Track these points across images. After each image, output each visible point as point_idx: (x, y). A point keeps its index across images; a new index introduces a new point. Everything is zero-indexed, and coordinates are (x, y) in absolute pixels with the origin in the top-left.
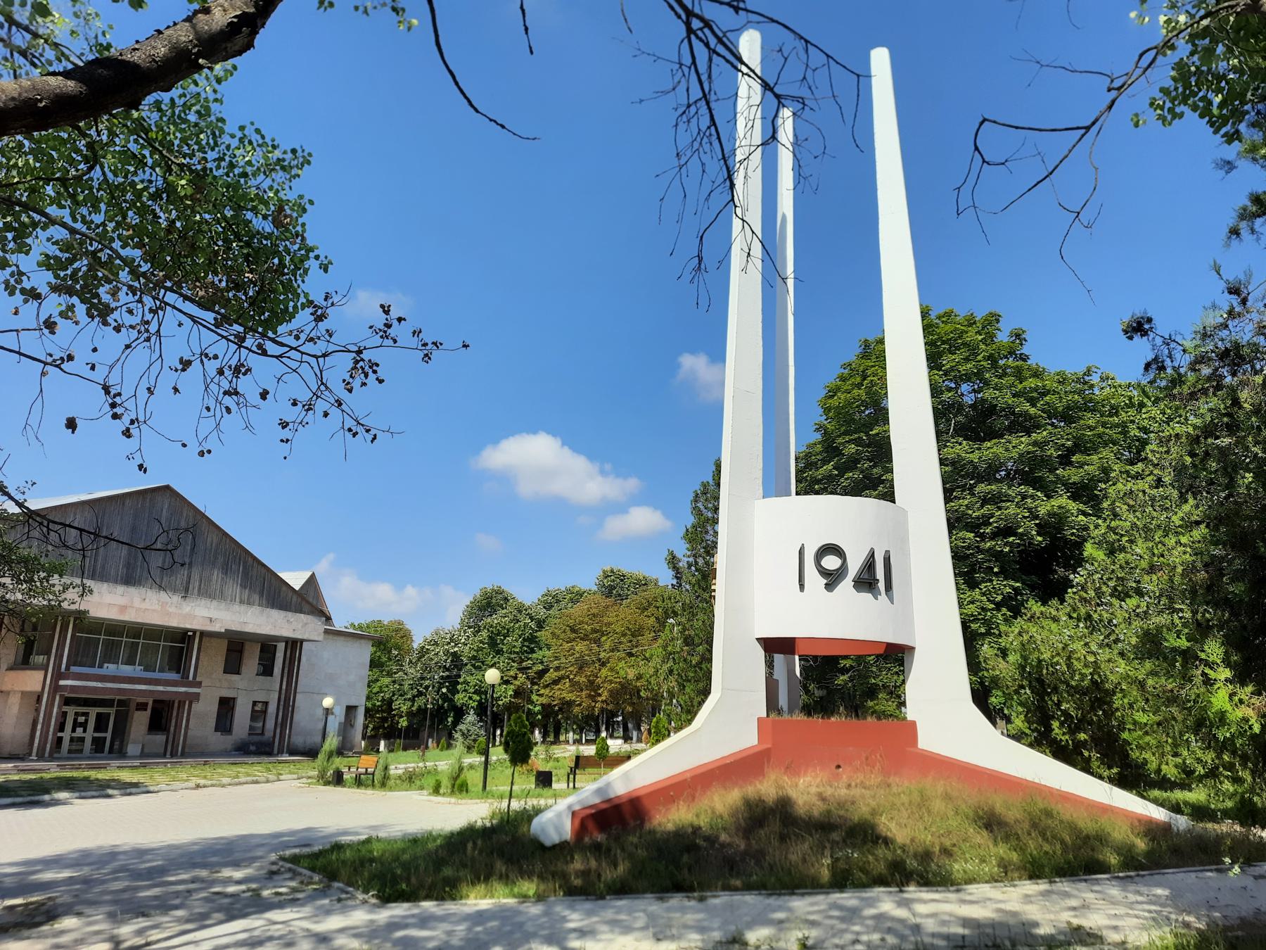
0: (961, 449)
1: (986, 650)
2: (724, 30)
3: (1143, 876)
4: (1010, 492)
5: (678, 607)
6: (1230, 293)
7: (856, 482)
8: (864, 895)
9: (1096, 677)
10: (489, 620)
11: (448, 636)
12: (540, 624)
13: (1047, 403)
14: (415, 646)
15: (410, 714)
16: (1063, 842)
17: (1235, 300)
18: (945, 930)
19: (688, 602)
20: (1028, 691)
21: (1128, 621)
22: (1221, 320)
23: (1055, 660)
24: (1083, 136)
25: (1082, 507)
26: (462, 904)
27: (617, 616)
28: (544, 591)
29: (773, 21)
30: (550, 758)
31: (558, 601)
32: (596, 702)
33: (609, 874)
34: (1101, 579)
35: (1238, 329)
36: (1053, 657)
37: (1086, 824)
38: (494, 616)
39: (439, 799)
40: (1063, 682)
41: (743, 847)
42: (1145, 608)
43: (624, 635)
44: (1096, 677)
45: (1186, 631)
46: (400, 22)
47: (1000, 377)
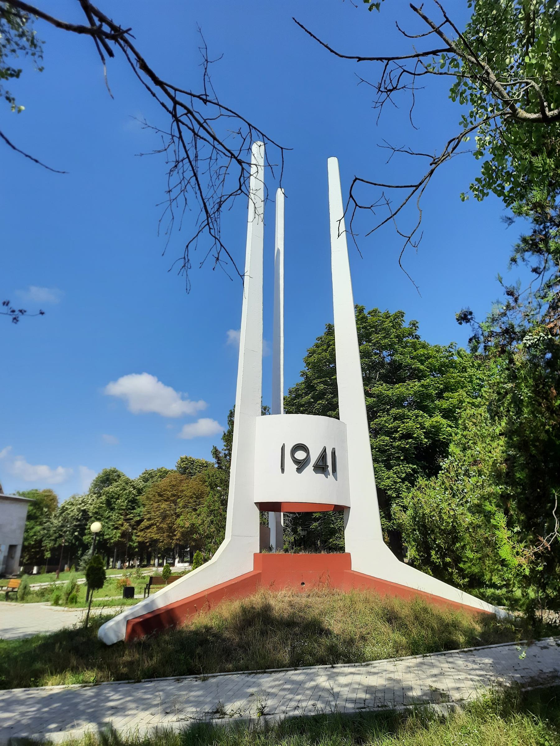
0: (381, 388)
1: (395, 508)
2: (205, 118)
3: (479, 650)
4: (409, 414)
5: (218, 481)
6: (508, 294)
7: (324, 406)
8: (309, 671)
9: (455, 524)
10: (107, 489)
11: (81, 499)
12: (140, 492)
13: (430, 363)
14: (60, 506)
15: (53, 550)
16: (433, 629)
17: (511, 299)
18: (354, 696)
19: (223, 478)
20: (418, 533)
21: (473, 490)
22: (502, 311)
23: (432, 514)
24: (414, 191)
25: (450, 423)
26: (41, 689)
27: (187, 486)
28: (144, 471)
29: (239, 117)
30: (140, 576)
31: (152, 477)
32: (173, 540)
33: (148, 664)
34: (458, 465)
35: (513, 317)
36: (431, 512)
37: (448, 618)
38: (110, 487)
39: (58, 608)
40: (437, 527)
41: (237, 640)
42: (481, 483)
43: (192, 498)
44: (455, 524)
45: (495, 500)
46: (13, 107)
47: (404, 348)
